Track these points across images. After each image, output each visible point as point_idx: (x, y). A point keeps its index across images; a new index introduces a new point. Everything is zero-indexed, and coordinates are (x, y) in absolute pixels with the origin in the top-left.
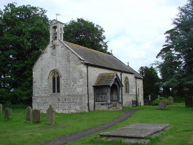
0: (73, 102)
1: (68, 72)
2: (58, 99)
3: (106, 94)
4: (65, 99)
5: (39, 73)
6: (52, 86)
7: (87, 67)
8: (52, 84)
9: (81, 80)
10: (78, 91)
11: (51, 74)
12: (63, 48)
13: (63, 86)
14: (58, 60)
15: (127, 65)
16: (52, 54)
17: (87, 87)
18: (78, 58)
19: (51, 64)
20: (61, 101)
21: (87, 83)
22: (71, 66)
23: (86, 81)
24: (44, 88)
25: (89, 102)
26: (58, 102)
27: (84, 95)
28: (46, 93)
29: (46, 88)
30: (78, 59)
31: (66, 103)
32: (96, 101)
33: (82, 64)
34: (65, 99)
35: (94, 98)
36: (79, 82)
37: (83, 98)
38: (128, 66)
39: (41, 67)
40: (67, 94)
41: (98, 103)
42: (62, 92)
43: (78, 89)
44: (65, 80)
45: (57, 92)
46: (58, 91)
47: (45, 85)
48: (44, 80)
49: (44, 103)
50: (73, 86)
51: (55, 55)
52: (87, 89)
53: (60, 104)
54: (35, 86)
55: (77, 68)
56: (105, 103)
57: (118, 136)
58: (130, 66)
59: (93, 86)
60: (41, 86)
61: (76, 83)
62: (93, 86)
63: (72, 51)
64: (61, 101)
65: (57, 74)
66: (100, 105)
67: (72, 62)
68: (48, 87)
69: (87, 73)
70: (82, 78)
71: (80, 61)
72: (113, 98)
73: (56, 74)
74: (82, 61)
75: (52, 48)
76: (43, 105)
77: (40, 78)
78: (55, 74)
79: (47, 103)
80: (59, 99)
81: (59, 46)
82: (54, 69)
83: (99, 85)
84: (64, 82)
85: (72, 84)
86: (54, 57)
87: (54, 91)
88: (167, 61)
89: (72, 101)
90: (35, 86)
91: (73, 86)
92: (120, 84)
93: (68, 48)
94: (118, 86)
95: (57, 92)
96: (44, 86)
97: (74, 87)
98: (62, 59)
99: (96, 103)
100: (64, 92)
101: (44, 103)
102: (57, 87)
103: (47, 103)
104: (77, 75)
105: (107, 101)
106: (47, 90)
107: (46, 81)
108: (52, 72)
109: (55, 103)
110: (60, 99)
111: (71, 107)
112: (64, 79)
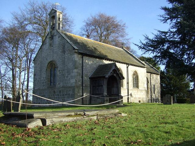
1: (64, 63)
3: (102, 86)
4: (60, 91)
7: (82, 57)
9: (75, 70)
11: (49, 66)
17: (81, 79)
21: (81, 74)
23: (81, 73)
27: (78, 87)
28: (44, 86)
29: (44, 80)
30: (73, 48)
33: (75, 54)
34: (60, 91)
35: (90, 91)
36: (73, 72)
37: (76, 90)
42: (58, 84)
43: (71, 80)
47: (43, 78)
51: (52, 46)
52: (81, 80)
53: (56, 96)
55: (71, 58)
59: (90, 78)
60: (40, 79)
62: (90, 78)
63: (67, 41)
66: (96, 98)
69: (82, 64)
70: (76, 68)
71: (74, 51)
72: (113, 92)
74: (76, 51)
80: (54, 92)
82: (51, 60)
83: (95, 76)
84: (60, 73)
86: (52, 47)
88: (172, 47)
92: (120, 76)
93: (64, 38)
94: (118, 78)
100: (59, 84)
102: (95, 106)
105: (103, 94)
108: (49, 64)
109: (51, 95)
112: (59, 71)
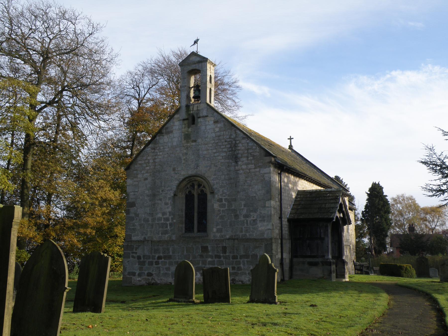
0: (246, 256)
2: (202, 247)
5: (147, 181)
6: (184, 215)
8: (184, 211)
10: (260, 229)
12: (219, 125)
13: (218, 217)
14: (205, 152)
15: (286, 145)
16: (187, 137)
18: (262, 151)
19: (183, 162)
20: (210, 254)
22: (243, 170)
24: (159, 219)
25: (284, 257)
26: (201, 256)
29: (167, 219)
31: (225, 258)
32: (296, 257)
34: (224, 249)
38: (291, 147)
39: (152, 167)
40: (228, 237)
41: (301, 260)
42: (215, 230)
43: (259, 224)
44: (224, 202)
45: (199, 231)
46: (203, 228)
47: (164, 214)
48: (160, 200)
49: (159, 258)
50: (246, 216)
51: (195, 141)
54: (133, 215)
56: (320, 260)
57: (423, 292)
58: (294, 148)
61: (255, 211)
64: (210, 254)
65: (199, 185)
67: (242, 159)
68: (172, 219)
71: (267, 159)
73: (196, 187)
75: (186, 122)
76: (157, 263)
77: (148, 196)
78: (193, 186)
79: (170, 257)
80: (205, 249)
81: (208, 119)
84: (223, 206)
85: (244, 212)
86: (194, 144)
87: (189, 228)
89: (242, 253)
90: (133, 215)
91: (246, 216)
95: (199, 231)
96: (160, 215)
97: (249, 219)
98: (214, 151)
99: (295, 260)
100: (219, 231)
101: (159, 258)
103: (170, 257)
104: (259, 190)
106: (171, 225)
107: (166, 204)
110: (209, 248)
111: (239, 269)
112: (220, 200)
